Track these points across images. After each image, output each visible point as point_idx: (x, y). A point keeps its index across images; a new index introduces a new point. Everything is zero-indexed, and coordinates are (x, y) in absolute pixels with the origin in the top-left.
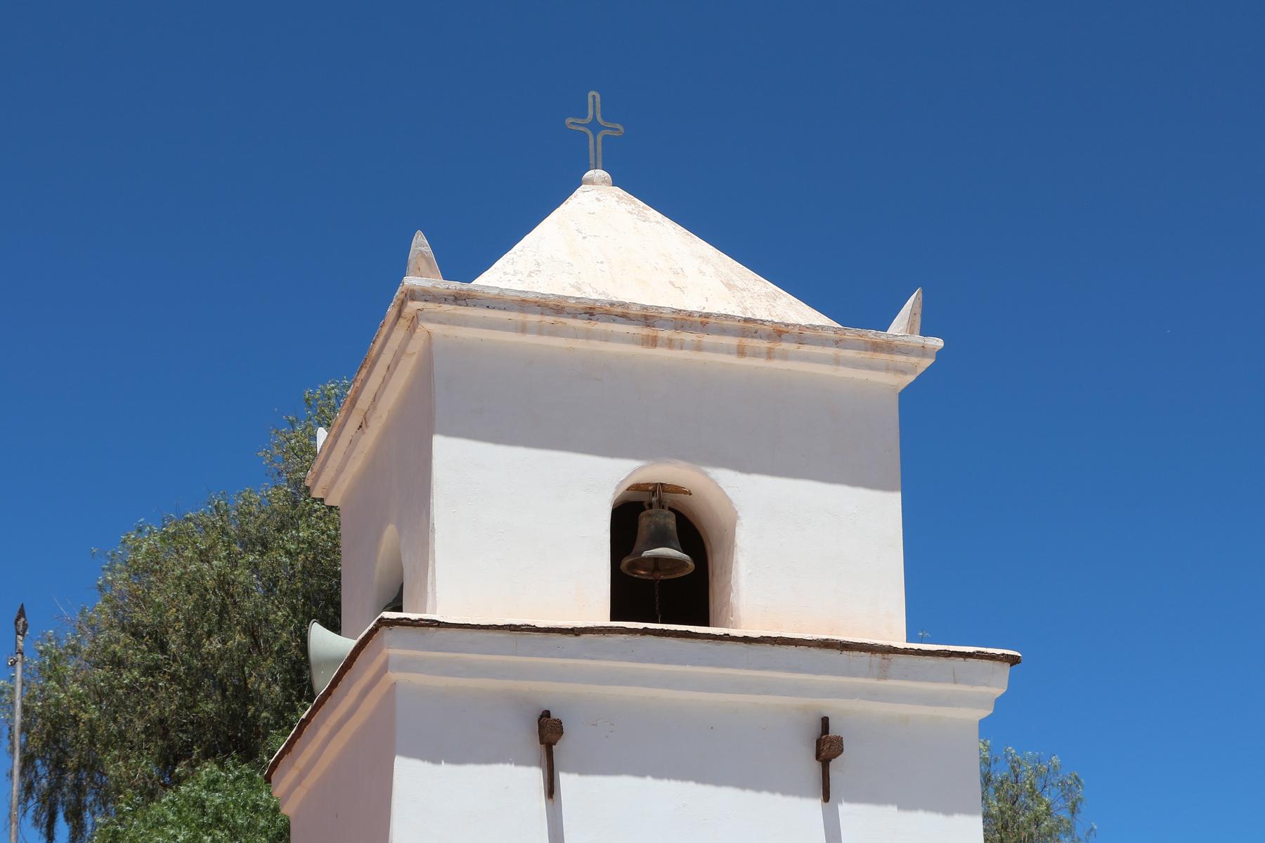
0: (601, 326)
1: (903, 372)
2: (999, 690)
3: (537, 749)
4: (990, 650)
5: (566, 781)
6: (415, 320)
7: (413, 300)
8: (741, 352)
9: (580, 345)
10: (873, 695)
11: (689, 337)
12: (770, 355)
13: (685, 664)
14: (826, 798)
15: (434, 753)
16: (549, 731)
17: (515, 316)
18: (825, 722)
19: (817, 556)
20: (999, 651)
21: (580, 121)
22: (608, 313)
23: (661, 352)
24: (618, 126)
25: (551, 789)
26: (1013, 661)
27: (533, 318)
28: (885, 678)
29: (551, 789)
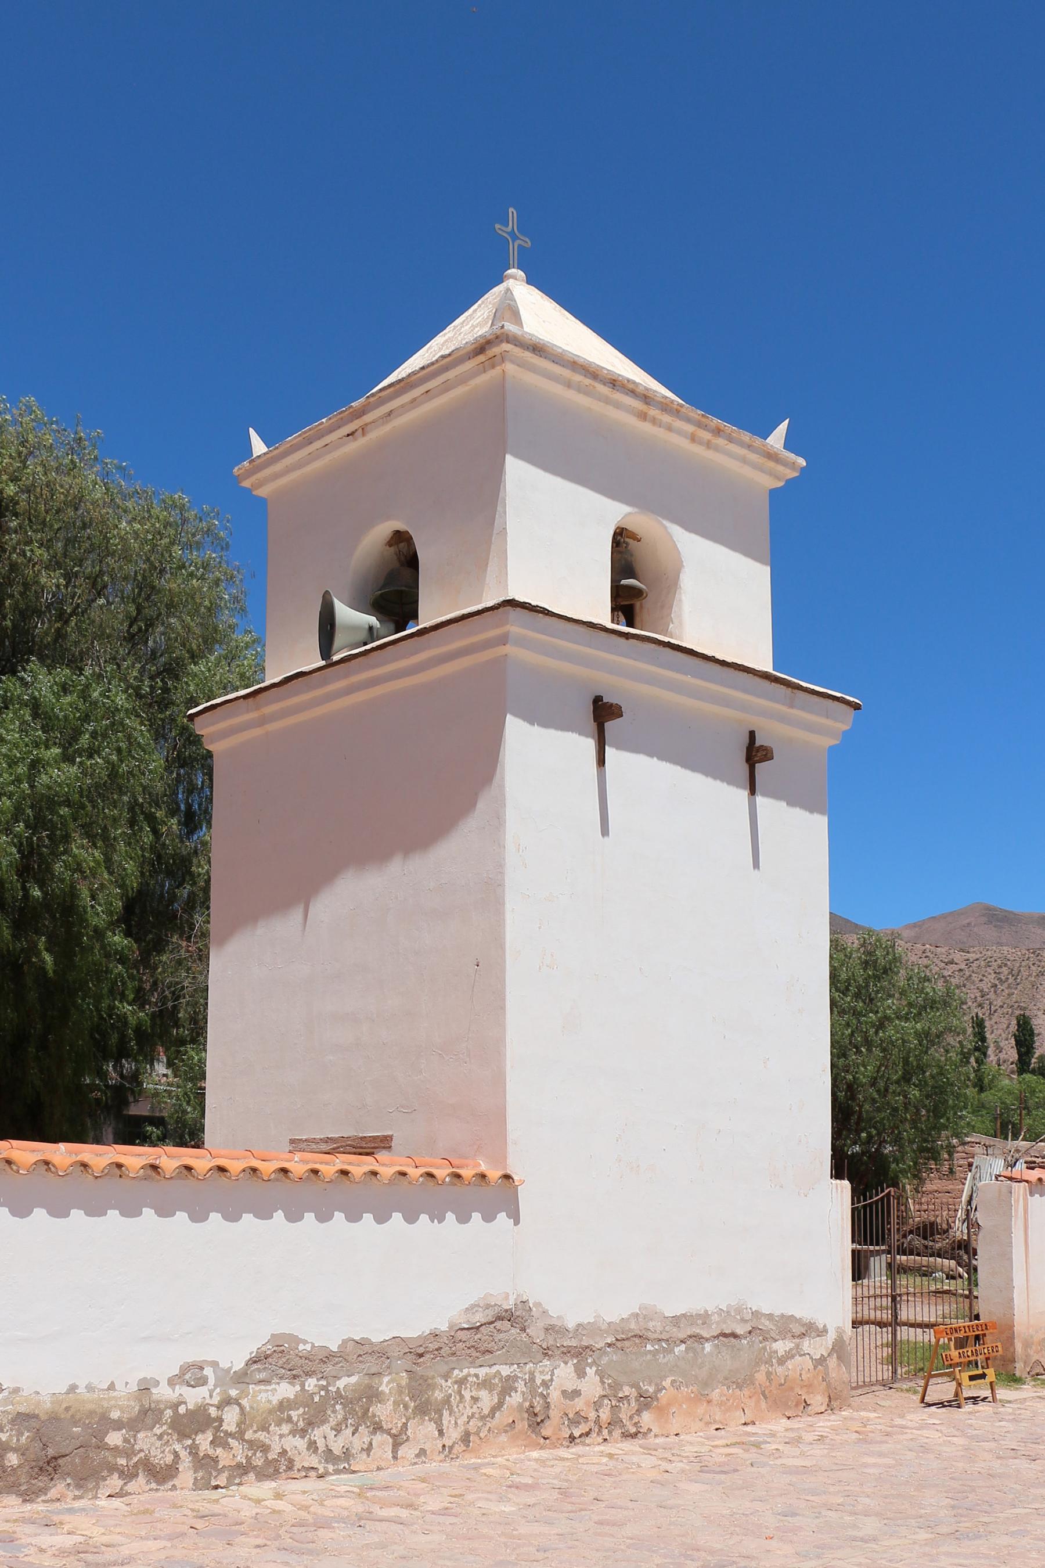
0: (618, 396)
1: (778, 478)
2: (845, 727)
3: (592, 726)
4: (848, 698)
5: (609, 751)
6: (503, 358)
7: (508, 342)
8: (693, 439)
9: (598, 407)
10: (783, 719)
11: (666, 418)
12: (708, 445)
13: (686, 674)
14: (753, 791)
15: (531, 718)
16: (603, 712)
17: (566, 373)
18: (752, 734)
19: (725, 603)
20: (838, 695)
21: (503, 228)
22: (623, 386)
23: (646, 427)
24: (527, 240)
25: (601, 761)
26: (857, 707)
27: (578, 378)
28: (791, 706)
29: (601, 761)
